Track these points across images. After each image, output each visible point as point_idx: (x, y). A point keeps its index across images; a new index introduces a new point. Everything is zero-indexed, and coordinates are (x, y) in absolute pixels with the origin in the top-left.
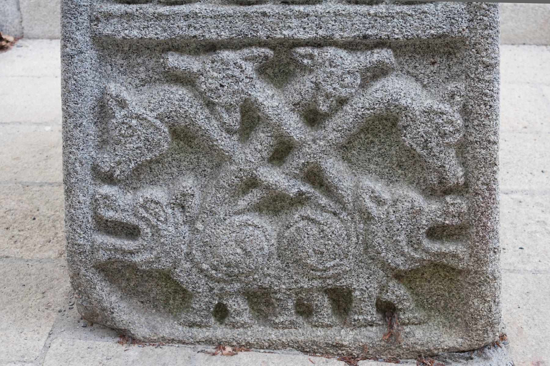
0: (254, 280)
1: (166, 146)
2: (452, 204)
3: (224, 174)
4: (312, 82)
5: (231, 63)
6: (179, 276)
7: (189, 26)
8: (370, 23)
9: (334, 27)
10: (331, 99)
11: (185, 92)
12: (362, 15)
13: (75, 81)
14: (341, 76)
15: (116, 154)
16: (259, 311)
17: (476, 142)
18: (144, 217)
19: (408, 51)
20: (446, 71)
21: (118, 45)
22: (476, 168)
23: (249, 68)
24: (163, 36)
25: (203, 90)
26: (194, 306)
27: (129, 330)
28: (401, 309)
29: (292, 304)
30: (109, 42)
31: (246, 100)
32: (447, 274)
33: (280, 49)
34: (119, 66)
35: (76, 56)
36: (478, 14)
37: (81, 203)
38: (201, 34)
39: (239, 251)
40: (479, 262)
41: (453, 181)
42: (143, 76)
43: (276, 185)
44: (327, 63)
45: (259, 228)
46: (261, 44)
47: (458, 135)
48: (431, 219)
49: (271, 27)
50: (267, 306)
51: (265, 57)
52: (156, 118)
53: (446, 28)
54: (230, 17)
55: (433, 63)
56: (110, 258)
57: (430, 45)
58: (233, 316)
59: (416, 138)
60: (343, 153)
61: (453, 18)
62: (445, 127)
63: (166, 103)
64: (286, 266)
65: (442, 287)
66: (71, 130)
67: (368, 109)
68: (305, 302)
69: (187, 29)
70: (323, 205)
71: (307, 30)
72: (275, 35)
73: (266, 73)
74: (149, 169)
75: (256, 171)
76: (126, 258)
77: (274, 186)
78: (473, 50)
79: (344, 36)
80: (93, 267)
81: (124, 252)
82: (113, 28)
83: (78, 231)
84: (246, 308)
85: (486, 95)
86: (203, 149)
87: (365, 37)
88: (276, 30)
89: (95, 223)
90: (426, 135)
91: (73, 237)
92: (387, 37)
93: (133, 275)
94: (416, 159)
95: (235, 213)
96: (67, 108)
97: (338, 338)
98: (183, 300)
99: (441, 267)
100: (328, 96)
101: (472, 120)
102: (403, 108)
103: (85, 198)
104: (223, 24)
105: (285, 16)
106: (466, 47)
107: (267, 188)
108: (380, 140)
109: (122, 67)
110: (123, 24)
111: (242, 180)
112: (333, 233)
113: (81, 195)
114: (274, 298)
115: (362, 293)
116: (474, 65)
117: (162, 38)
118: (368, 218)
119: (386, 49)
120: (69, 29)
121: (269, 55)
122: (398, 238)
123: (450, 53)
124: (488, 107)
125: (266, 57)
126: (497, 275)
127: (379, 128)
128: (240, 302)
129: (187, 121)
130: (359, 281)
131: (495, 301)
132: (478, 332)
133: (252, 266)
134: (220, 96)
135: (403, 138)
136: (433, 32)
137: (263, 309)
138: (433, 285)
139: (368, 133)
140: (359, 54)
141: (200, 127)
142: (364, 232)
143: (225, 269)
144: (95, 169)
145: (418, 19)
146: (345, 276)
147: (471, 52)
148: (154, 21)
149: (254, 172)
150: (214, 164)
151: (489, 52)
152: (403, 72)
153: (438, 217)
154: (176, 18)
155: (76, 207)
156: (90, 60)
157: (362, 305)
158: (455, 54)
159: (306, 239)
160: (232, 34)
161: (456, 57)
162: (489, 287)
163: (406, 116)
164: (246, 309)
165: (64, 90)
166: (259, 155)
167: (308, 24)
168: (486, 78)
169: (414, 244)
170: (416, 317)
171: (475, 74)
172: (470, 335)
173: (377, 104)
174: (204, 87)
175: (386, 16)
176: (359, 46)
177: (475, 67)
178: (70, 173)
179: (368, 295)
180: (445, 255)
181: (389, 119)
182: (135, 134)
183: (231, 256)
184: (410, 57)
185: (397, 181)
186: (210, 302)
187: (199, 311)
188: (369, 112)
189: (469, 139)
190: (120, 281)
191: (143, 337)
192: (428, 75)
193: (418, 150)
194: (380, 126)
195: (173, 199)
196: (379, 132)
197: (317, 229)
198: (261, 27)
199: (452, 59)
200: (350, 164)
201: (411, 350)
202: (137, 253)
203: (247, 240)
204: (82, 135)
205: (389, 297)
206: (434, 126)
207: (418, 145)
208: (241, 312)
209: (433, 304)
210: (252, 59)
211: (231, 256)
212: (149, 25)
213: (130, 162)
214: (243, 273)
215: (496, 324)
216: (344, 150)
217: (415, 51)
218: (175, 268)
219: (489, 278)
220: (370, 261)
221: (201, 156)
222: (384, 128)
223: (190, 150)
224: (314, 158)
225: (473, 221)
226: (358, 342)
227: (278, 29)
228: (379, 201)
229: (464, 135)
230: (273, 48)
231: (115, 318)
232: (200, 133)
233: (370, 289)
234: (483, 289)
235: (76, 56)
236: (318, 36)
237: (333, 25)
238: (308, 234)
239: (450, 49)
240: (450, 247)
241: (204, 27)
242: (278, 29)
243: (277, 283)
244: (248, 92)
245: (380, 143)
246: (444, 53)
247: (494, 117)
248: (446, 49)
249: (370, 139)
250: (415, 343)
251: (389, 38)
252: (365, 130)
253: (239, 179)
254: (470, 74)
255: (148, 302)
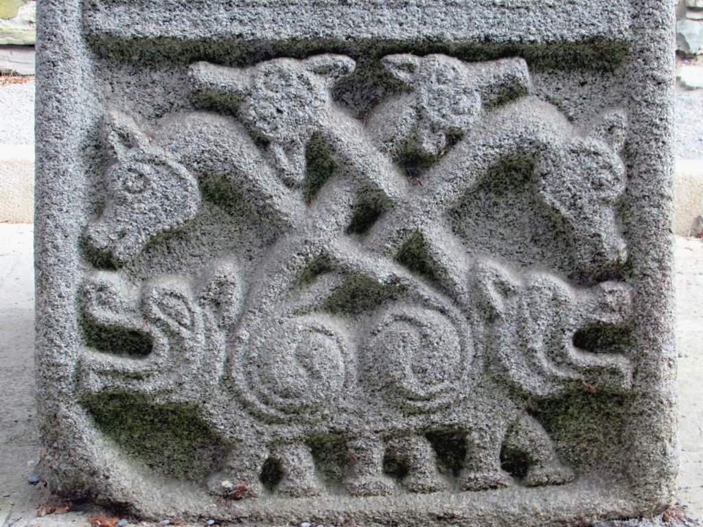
0: (324, 417)
1: (193, 209)
2: (610, 292)
3: (279, 252)
4: (411, 107)
5: (294, 76)
6: (211, 414)
7: (232, 19)
8: (495, 18)
9: (445, 22)
10: (439, 133)
11: (223, 124)
12: (484, 5)
13: (59, 101)
14: (454, 97)
15: (118, 221)
16: (329, 473)
17: (644, 196)
18: (159, 319)
19: (546, 66)
20: (600, 96)
21: (122, 53)
22: (643, 236)
23: (322, 86)
24: (194, 33)
25: (251, 118)
26: (231, 464)
27: (132, 505)
28: (537, 461)
29: (379, 456)
30: (109, 46)
31: (314, 136)
32: (602, 406)
33: (363, 60)
34: (125, 85)
35: (60, 63)
36: (646, 6)
37: (63, 297)
38: (250, 32)
39: (302, 371)
40: (648, 379)
41: (612, 258)
42: (160, 100)
43: (357, 265)
44: (434, 78)
45: (331, 335)
46: (337, 50)
47: (619, 186)
48: (581, 315)
49: (353, 22)
50: (341, 465)
51: (343, 68)
52: (180, 162)
53: (603, 27)
54: (292, 4)
55: (583, 84)
56: (106, 387)
57: (578, 57)
58: (291, 477)
59: (559, 192)
60: (453, 222)
61: (612, 12)
62: (600, 174)
63: (195, 139)
64: (371, 395)
65: (595, 427)
66: (50, 181)
67: (492, 147)
68: (398, 453)
69: (229, 24)
70: (426, 297)
71: (405, 26)
72: (358, 34)
73: (343, 100)
74: (166, 250)
75: (328, 246)
76: (130, 386)
77: (355, 268)
78: (639, 60)
79: (459, 37)
80: (78, 402)
81: (127, 376)
82: (118, 22)
83: (58, 342)
84: (310, 465)
85: (657, 127)
86: (248, 218)
87: (487, 39)
88: (360, 27)
89: (82, 331)
90: (574, 187)
91: (49, 353)
92: (519, 39)
93: (139, 421)
94: (557, 230)
95: (296, 313)
96: (44, 146)
97: (447, 505)
98: (214, 460)
99: (593, 396)
100: (434, 128)
101: (639, 164)
102: (541, 147)
103: (68, 290)
104: (283, 16)
105: (373, 4)
106: (629, 57)
107: (345, 272)
108: (507, 202)
109: (128, 87)
110: (133, 15)
111: (307, 260)
112: (440, 339)
113: (64, 284)
114: (352, 447)
115: (482, 436)
116: (640, 81)
117: (192, 37)
118: (492, 317)
119: (517, 58)
120: (51, 20)
121: (350, 65)
122: (534, 345)
123: (605, 70)
124: (661, 144)
125: (345, 70)
126: (674, 400)
127: (506, 183)
128: (302, 455)
129: (227, 167)
130: (477, 417)
131: (670, 440)
132: (648, 487)
133: (322, 395)
134: (277, 128)
135: (542, 192)
136: (583, 32)
137: (334, 469)
138: (582, 425)
139: (490, 190)
140: (478, 65)
141: (246, 177)
142: (485, 340)
143: (281, 400)
144: (85, 245)
145: (563, 12)
146: (456, 409)
147: (636, 64)
148: (180, 11)
149: (326, 246)
150: (265, 240)
151: (661, 62)
152: (541, 97)
153: (590, 313)
154: (212, 7)
155: (56, 303)
156: (81, 72)
157: (481, 455)
158: (613, 71)
159: (401, 349)
160: (296, 31)
161: (614, 76)
162: (662, 417)
163: (546, 159)
164: (310, 468)
165: (41, 117)
166: (333, 220)
167: (407, 18)
168: (657, 102)
169: (557, 356)
170: (559, 472)
171: (643, 96)
172: (636, 493)
173: (504, 139)
174: (253, 113)
175: (518, 8)
176: (479, 55)
177: (641, 84)
178: (47, 250)
179: (491, 438)
180: (600, 370)
181: (520, 169)
182: (148, 187)
183: (289, 379)
184: (549, 74)
185: (531, 263)
186: (257, 456)
187: (240, 471)
188: (492, 152)
189: (634, 193)
190: (118, 431)
191: (155, 514)
192: (575, 103)
193: (563, 211)
194: (507, 179)
195: (204, 291)
196: (506, 189)
197: (418, 334)
198: (338, 21)
199: (608, 78)
200: (463, 240)
201: (552, 518)
202: (148, 377)
203: (314, 352)
204: (66, 188)
205: (520, 442)
206: (585, 172)
207: (563, 203)
208: (302, 472)
209: (582, 454)
210: (321, 72)
211: (289, 379)
212: (173, 17)
213: (139, 233)
214: (307, 406)
215: (672, 474)
216: (455, 218)
217: (557, 66)
218: (204, 402)
219: (662, 403)
220: (493, 385)
221: (245, 228)
222: (513, 184)
223: (229, 218)
224: (414, 222)
225: (640, 317)
226: (477, 510)
227: (362, 25)
228: (506, 291)
229: (627, 190)
230: (355, 58)
231: (110, 485)
232: (246, 186)
233: (493, 429)
234: (655, 420)
235: (60, 63)
236: (422, 37)
237: (442, 20)
238: (404, 342)
239: (606, 64)
240: (604, 360)
241: (254, 20)
242: (362, 25)
243: (357, 423)
244: (317, 122)
245: (506, 205)
246: (598, 69)
247: (669, 160)
248: (600, 63)
249: (493, 200)
250: (558, 508)
251: (521, 41)
252: (484, 186)
253: (302, 257)
254: (634, 96)
255: (160, 465)
